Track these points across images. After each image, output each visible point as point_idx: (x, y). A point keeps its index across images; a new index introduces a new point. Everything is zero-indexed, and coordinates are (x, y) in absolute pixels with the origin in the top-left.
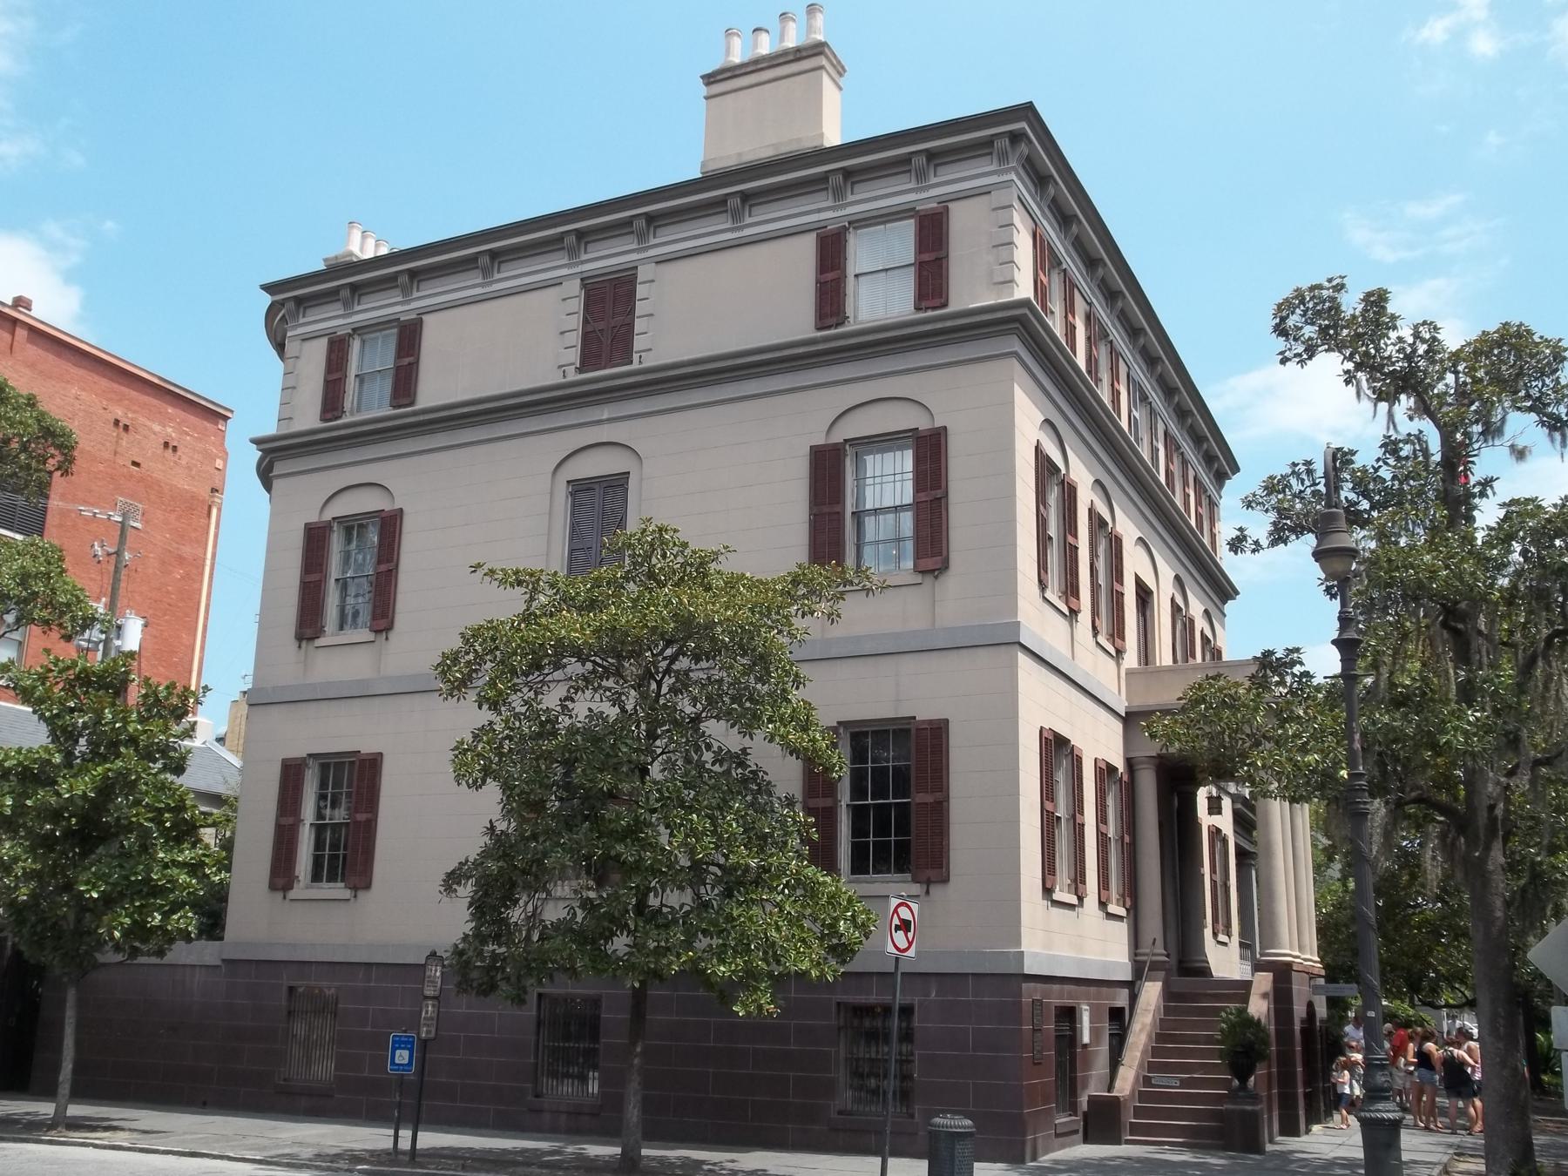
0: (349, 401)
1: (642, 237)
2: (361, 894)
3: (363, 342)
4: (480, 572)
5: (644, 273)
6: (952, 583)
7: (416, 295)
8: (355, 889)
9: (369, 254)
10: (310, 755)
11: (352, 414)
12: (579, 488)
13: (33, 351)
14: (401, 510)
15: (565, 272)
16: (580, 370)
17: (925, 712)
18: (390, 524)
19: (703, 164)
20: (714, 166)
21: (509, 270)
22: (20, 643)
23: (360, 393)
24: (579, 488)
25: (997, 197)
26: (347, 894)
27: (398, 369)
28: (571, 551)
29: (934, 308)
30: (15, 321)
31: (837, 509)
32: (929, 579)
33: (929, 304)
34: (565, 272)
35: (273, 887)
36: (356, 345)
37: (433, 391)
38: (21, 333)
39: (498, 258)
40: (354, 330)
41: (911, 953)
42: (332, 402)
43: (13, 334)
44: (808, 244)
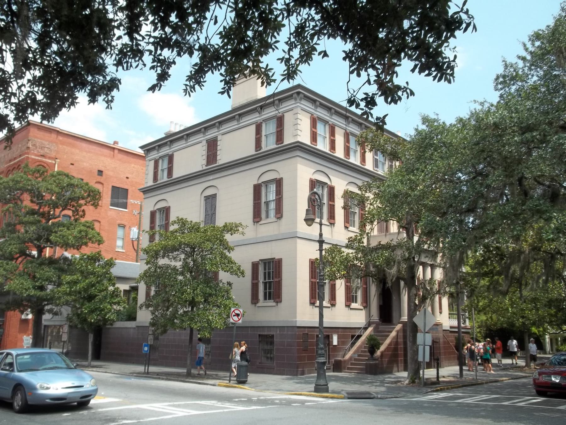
0: (263, 144)
1: (218, 128)
2: (279, 304)
3: (266, 124)
4: (145, 232)
5: (219, 138)
6: (283, 220)
7: (189, 141)
8: (277, 302)
9: (177, 130)
10: (260, 260)
11: (160, 180)
12: (207, 198)
13: (120, 156)
14: (282, 178)
15: (202, 139)
16: (206, 166)
17: (277, 257)
18: (279, 183)
19: (232, 106)
20: (233, 107)
21: (224, 126)
22: (123, 239)
23: (267, 140)
24: (207, 198)
25: (295, 111)
26: (274, 304)
27: (277, 132)
28: (205, 215)
29: (280, 144)
30: (114, 148)
31: (259, 201)
32: (279, 220)
33: (279, 143)
34: (202, 139)
35: (252, 303)
36: (264, 125)
37: (177, 174)
38: (116, 151)
39: (188, 135)
40: (160, 157)
41: (240, 321)
42: (155, 178)
43: (114, 152)
44: (253, 127)
